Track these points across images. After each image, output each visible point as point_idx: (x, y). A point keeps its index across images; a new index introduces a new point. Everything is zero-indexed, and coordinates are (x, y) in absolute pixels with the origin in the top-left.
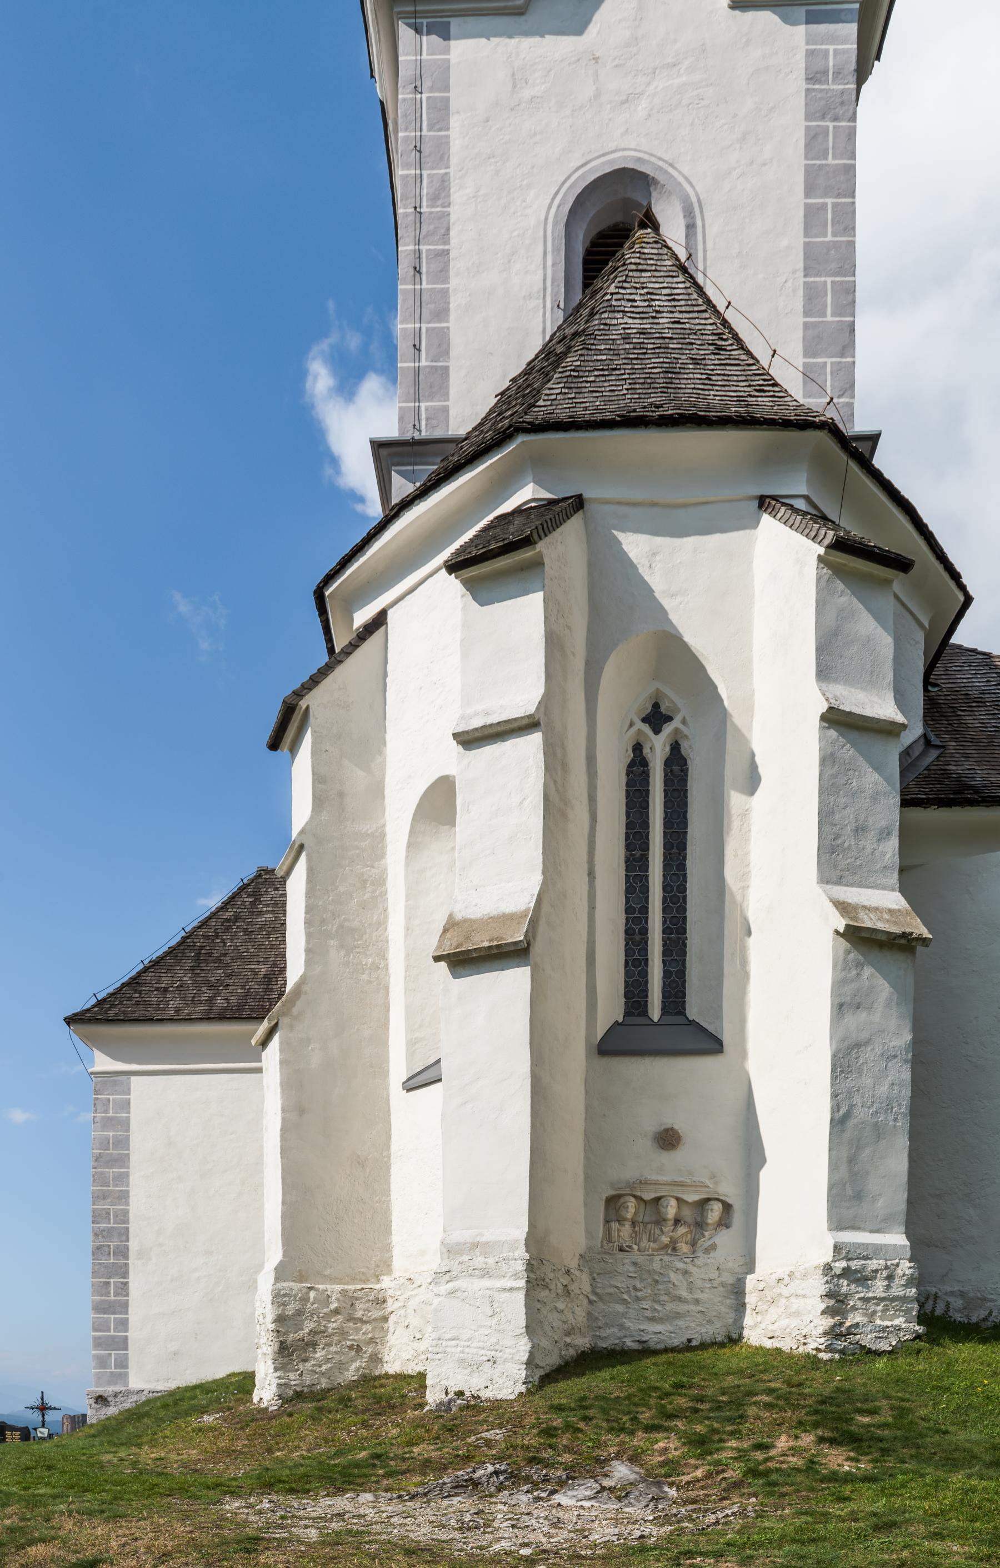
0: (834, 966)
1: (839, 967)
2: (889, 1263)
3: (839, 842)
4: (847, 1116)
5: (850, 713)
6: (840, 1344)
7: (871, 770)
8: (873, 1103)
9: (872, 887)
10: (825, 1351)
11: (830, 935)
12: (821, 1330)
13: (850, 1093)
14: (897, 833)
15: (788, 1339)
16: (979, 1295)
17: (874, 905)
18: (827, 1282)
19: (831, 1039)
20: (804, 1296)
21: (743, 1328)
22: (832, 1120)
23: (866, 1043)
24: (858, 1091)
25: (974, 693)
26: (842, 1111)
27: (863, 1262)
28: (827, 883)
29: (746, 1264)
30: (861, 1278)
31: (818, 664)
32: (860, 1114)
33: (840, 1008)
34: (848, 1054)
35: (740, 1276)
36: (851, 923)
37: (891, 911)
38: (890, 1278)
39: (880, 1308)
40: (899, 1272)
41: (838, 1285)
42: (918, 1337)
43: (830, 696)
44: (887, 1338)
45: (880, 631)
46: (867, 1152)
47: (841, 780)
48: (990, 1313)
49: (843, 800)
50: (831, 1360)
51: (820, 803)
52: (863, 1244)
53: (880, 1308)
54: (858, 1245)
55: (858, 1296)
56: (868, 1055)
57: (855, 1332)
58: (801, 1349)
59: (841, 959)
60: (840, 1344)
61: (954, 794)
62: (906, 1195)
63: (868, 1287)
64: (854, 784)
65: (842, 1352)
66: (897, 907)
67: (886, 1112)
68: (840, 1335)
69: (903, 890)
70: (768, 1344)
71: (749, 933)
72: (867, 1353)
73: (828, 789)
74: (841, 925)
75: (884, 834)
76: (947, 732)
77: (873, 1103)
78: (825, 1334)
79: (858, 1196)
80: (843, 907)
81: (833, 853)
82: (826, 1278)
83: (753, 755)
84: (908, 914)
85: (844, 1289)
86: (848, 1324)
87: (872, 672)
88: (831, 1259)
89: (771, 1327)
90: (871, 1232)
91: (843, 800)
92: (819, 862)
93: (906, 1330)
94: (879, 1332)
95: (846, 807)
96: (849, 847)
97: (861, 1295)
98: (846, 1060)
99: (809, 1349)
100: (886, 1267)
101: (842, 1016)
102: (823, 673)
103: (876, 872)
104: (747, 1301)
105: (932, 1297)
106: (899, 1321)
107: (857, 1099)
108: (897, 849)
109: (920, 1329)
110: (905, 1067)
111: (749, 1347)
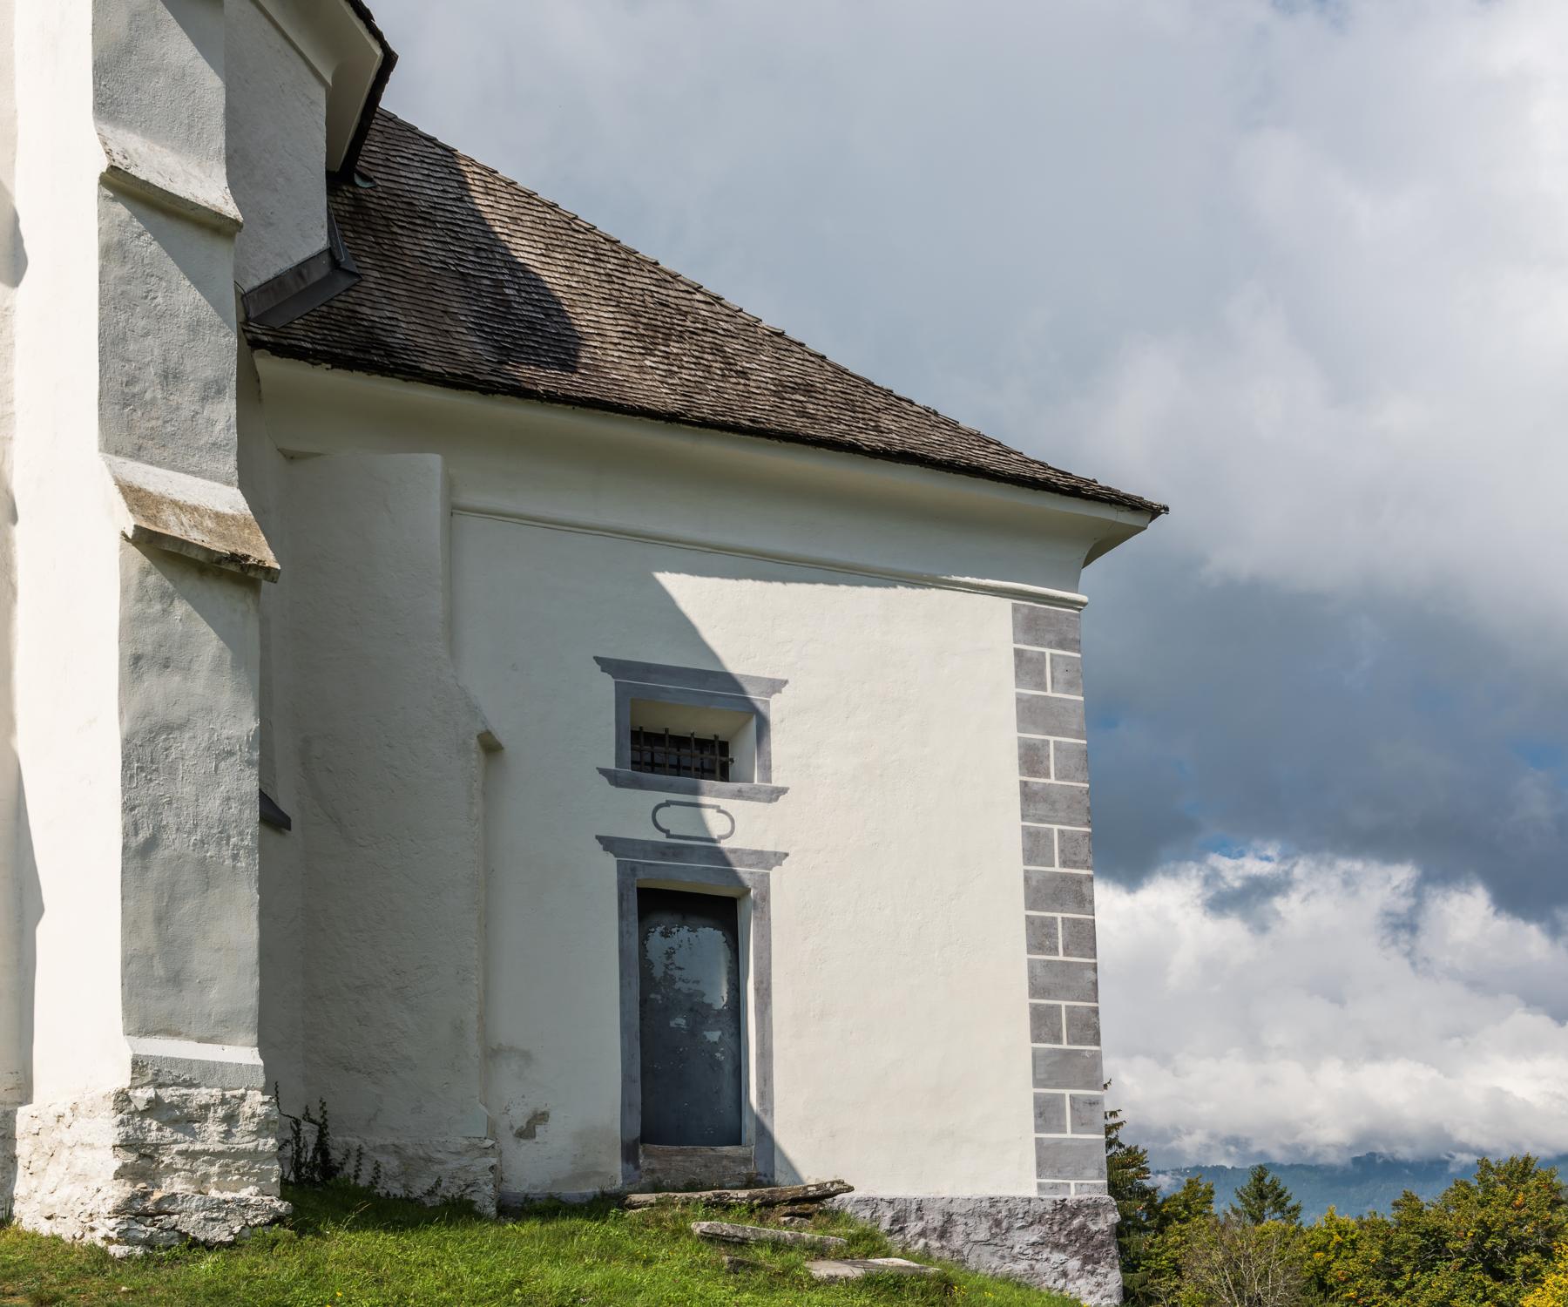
0: (124, 591)
1: (132, 595)
2: (228, 1094)
3: (136, 389)
4: (151, 844)
5: (146, 183)
6: (144, 1230)
7: (188, 283)
8: (196, 826)
9: (193, 473)
10: (118, 1242)
11: (117, 541)
12: (110, 1206)
13: (155, 806)
14: (234, 393)
15: (70, 1221)
16: (421, 1153)
17: (192, 501)
18: (122, 1123)
19: (121, 713)
20: (91, 1146)
21: (13, 1200)
22: (125, 848)
23: (181, 727)
24: (170, 803)
25: (422, 205)
26: (144, 835)
27: (184, 1091)
28: (117, 453)
29: (19, 1087)
30: (184, 1120)
31: (97, 93)
32: (175, 843)
33: (134, 664)
34: (151, 740)
35: (9, 1108)
36: (144, 525)
37: (218, 517)
38: (230, 1119)
39: (215, 1169)
40: (246, 1109)
41: (141, 1128)
42: (278, 1219)
43: (115, 148)
44: (224, 1220)
45: (202, 65)
46: (188, 906)
47: (137, 290)
48: (438, 1183)
49: (142, 323)
50: (129, 1257)
51: (101, 320)
52: (183, 1061)
53: (215, 1169)
54: (175, 1062)
55: (176, 1148)
56: (187, 746)
57: (170, 1209)
58: (88, 1237)
59: (135, 581)
60: (144, 1230)
61: (355, 350)
62: (257, 982)
63: (194, 1134)
64: (159, 300)
65: (149, 1243)
66: (230, 512)
67: (219, 844)
68: (144, 1215)
69: (247, 483)
70: (46, 1228)
71: (14, 518)
72: (190, 1247)
73: (114, 301)
74: (129, 523)
75: (210, 391)
76: (371, 255)
77: (196, 826)
78: (118, 1212)
79: (176, 980)
80: (135, 496)
81: (126, 405)
82: (120, 1116)
83: (16, 219)
84: (247, 525)
85: (153, 1136)
86: (157, 1195)
87: (190, 127)
88: (128, 1083)
89: (50, 1200)
90: (200, 1040)
91: (142, 323)
92: (101, 416)
93: (258, 1207)
94: (211, 1209)
95: (147, 335)
96: (153, 401)
97: (183, 1147)
98: (148, 750)
99: (97, 1238)
100: (224, 1101)
101: (140, 677)
102: (107, 107)
103: (200, 449)
104: (17, 1152)
105: (354, 1154)
106: (248, 1193)
107: (168, 818)
108: (233, 419)
109: (281, 1206)
110: (247, 772)
111: (19, 1234)
